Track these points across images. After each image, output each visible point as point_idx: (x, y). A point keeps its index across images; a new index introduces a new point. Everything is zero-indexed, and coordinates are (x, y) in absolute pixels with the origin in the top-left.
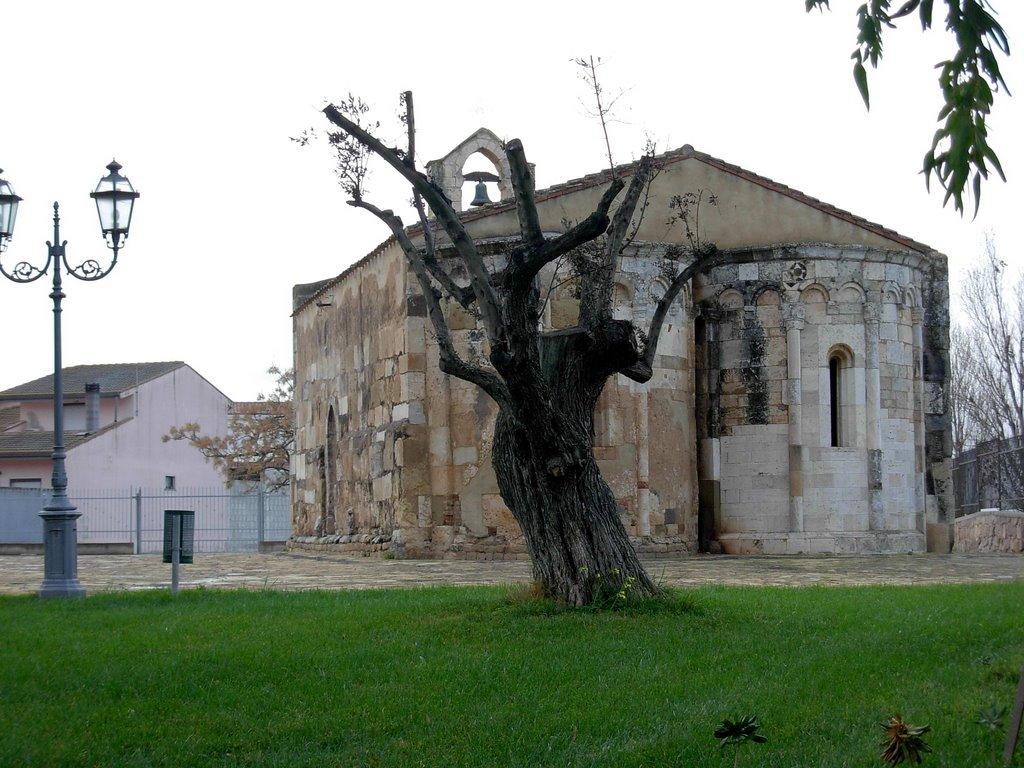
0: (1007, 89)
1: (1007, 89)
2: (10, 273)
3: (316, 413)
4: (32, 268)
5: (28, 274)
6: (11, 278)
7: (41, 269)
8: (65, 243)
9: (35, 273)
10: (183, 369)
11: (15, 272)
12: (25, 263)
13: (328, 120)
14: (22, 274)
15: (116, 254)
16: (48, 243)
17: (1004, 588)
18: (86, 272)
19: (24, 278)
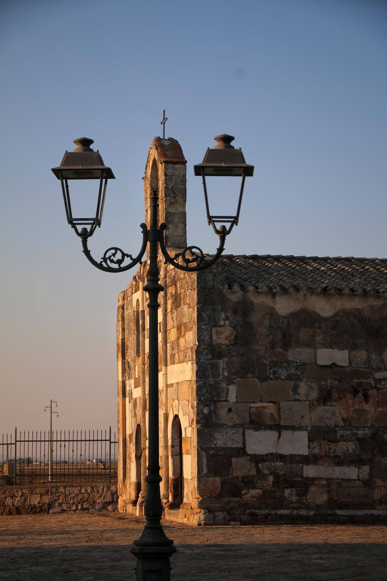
0: (16, 430)
1: (16, 430)
2: (98, 260)
3: (25, 569)
4: (124, 255)
5: (120, 262)
6: (99, 266)
7: (135, 256)
8: (209, 225)
9: (127, 261)
10: (137, 398)
11: (105, 259)
12: (116, 249)
13: (177, 140)
14: (112, 261)
15: (223, 240)
16: (143, 226)
17: (381, 526)
18: (187, 261)
19: (116, 266)
